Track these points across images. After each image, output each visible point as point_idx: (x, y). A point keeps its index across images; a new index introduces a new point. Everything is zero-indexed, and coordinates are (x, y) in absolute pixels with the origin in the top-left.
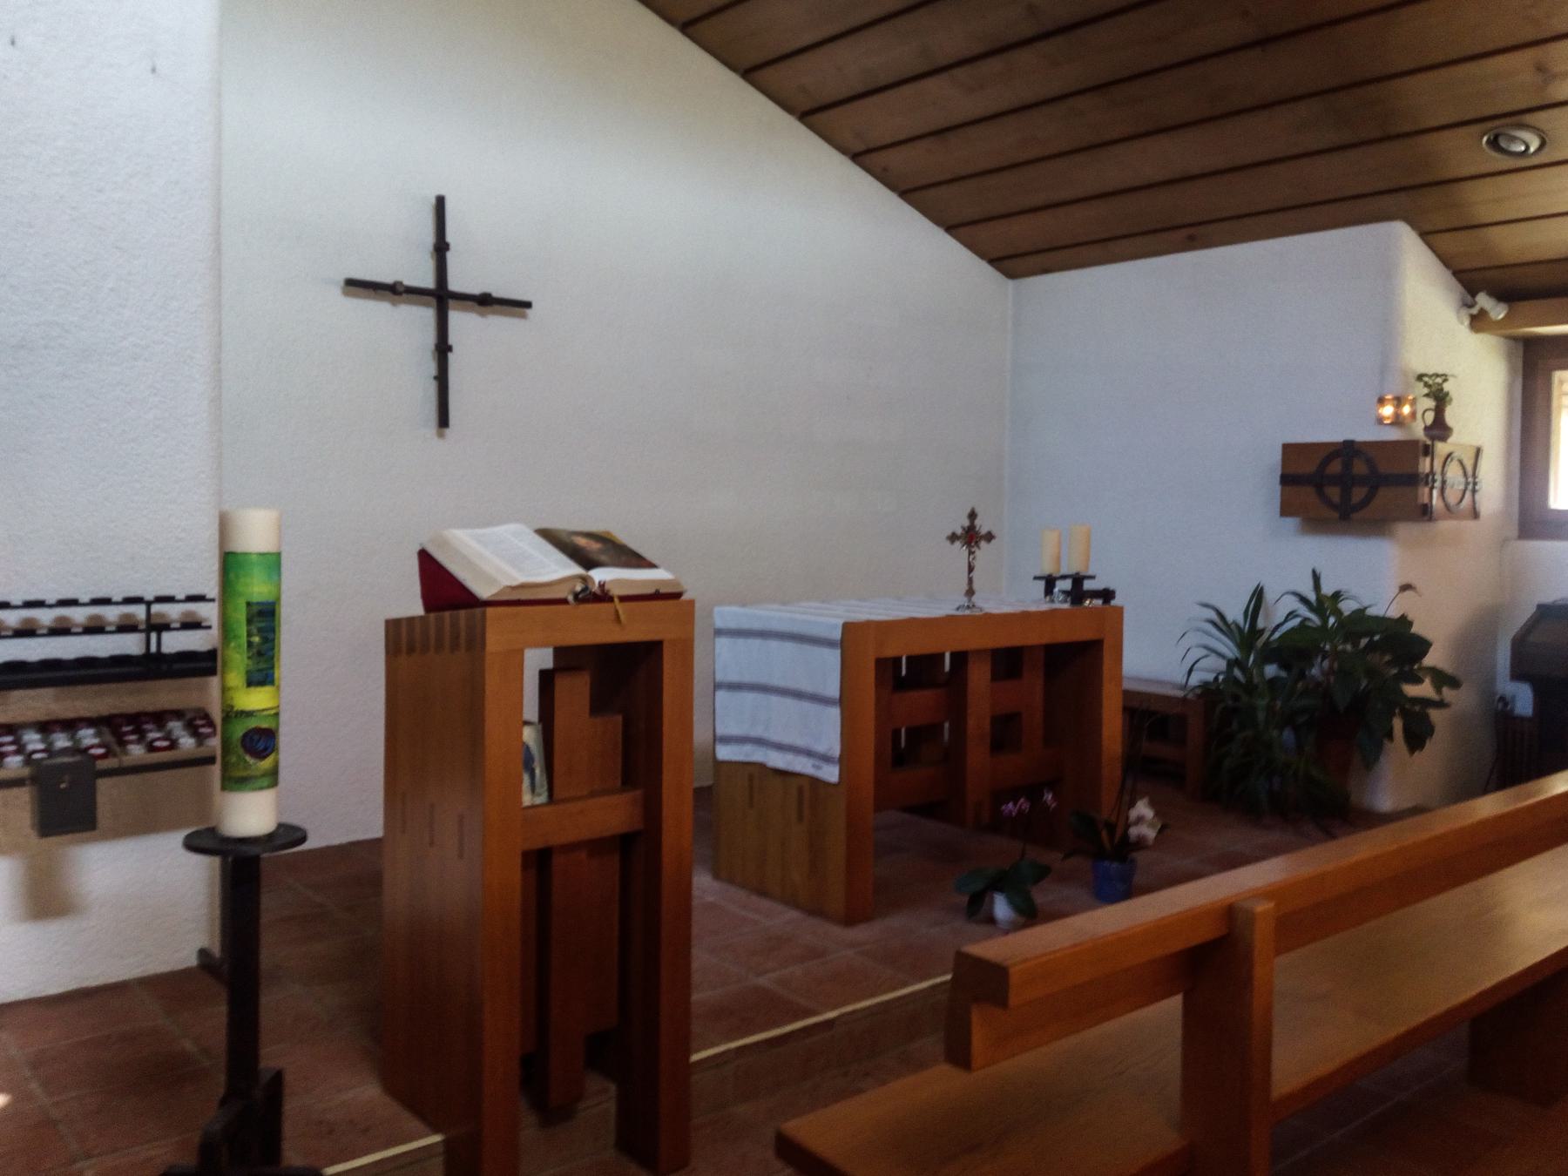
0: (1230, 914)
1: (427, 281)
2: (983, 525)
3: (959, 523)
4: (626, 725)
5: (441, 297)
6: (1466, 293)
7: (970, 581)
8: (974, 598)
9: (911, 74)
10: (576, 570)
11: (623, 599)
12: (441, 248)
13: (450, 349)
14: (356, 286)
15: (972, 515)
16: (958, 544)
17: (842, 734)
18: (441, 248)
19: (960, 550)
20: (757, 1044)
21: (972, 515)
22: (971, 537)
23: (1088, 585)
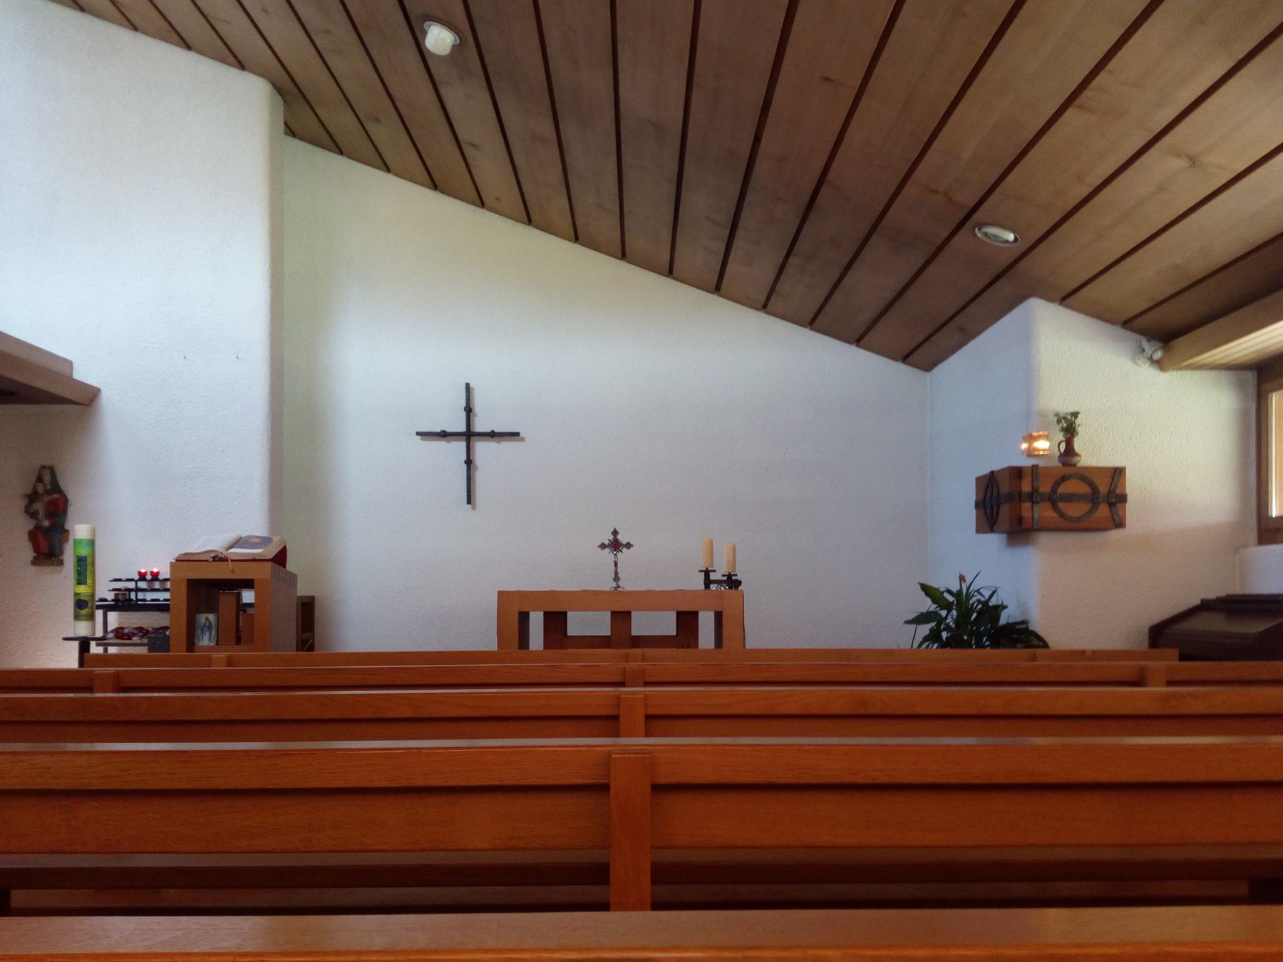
0: (648, 734)
1: (463, 429)
2: (622, 538)
3: (607, 538)
4: (744, 647)
5: (469, 435)
6: (970, 208)
7: (616, 573)
8: (619, 583)
9: (420, 59)
10: (933, 607)
11: (232, 561)
12: (469, 410)
13: (466, 462)
14: (424, 435)
15: (615, 533)
16: (607, 550)
17: (759, 650)
18: (469, 410)
19: (608, 555)
20: (246, 752)
21: (615, 533)
22: (615, 545)
23: (713, 576)
